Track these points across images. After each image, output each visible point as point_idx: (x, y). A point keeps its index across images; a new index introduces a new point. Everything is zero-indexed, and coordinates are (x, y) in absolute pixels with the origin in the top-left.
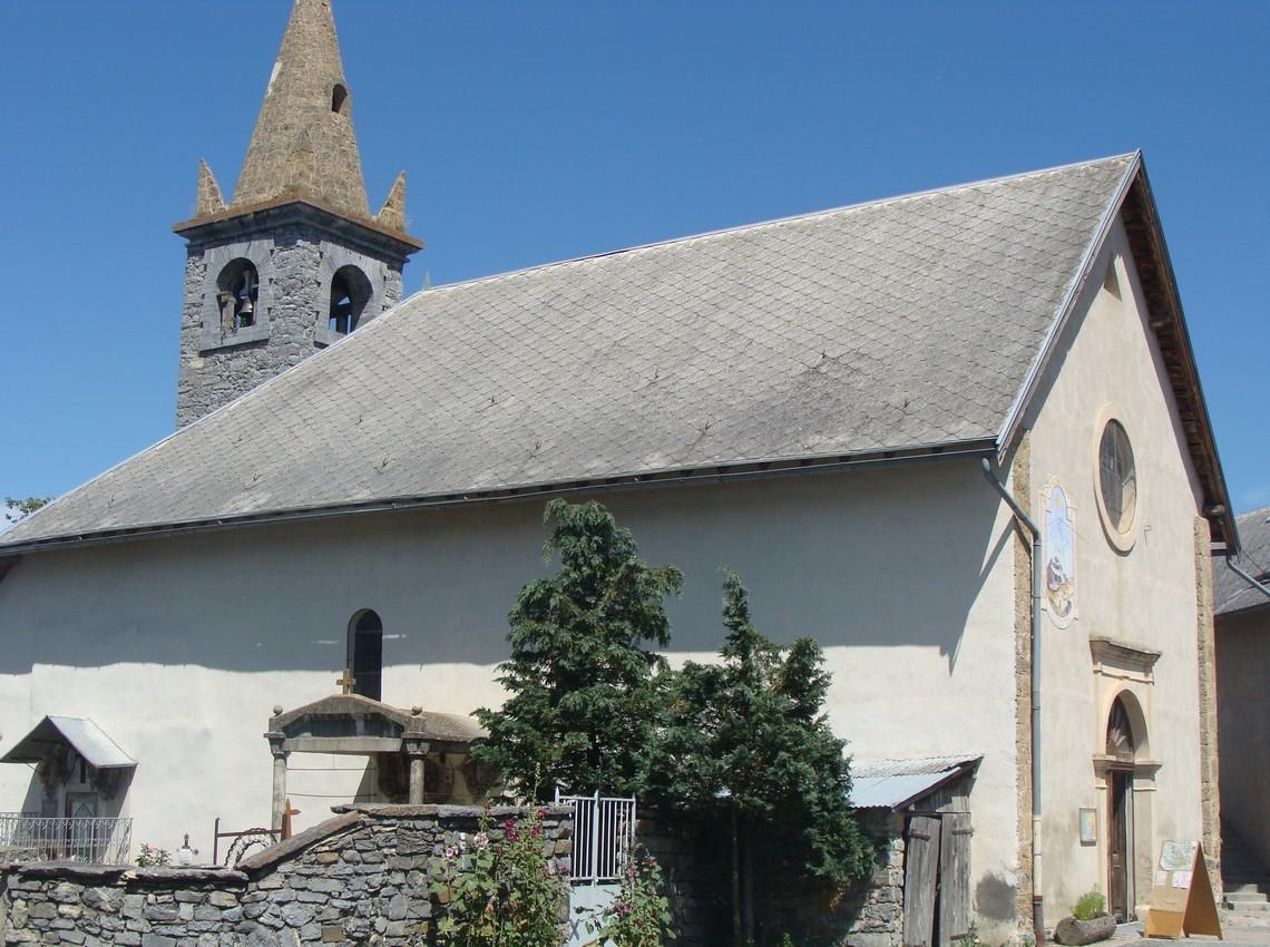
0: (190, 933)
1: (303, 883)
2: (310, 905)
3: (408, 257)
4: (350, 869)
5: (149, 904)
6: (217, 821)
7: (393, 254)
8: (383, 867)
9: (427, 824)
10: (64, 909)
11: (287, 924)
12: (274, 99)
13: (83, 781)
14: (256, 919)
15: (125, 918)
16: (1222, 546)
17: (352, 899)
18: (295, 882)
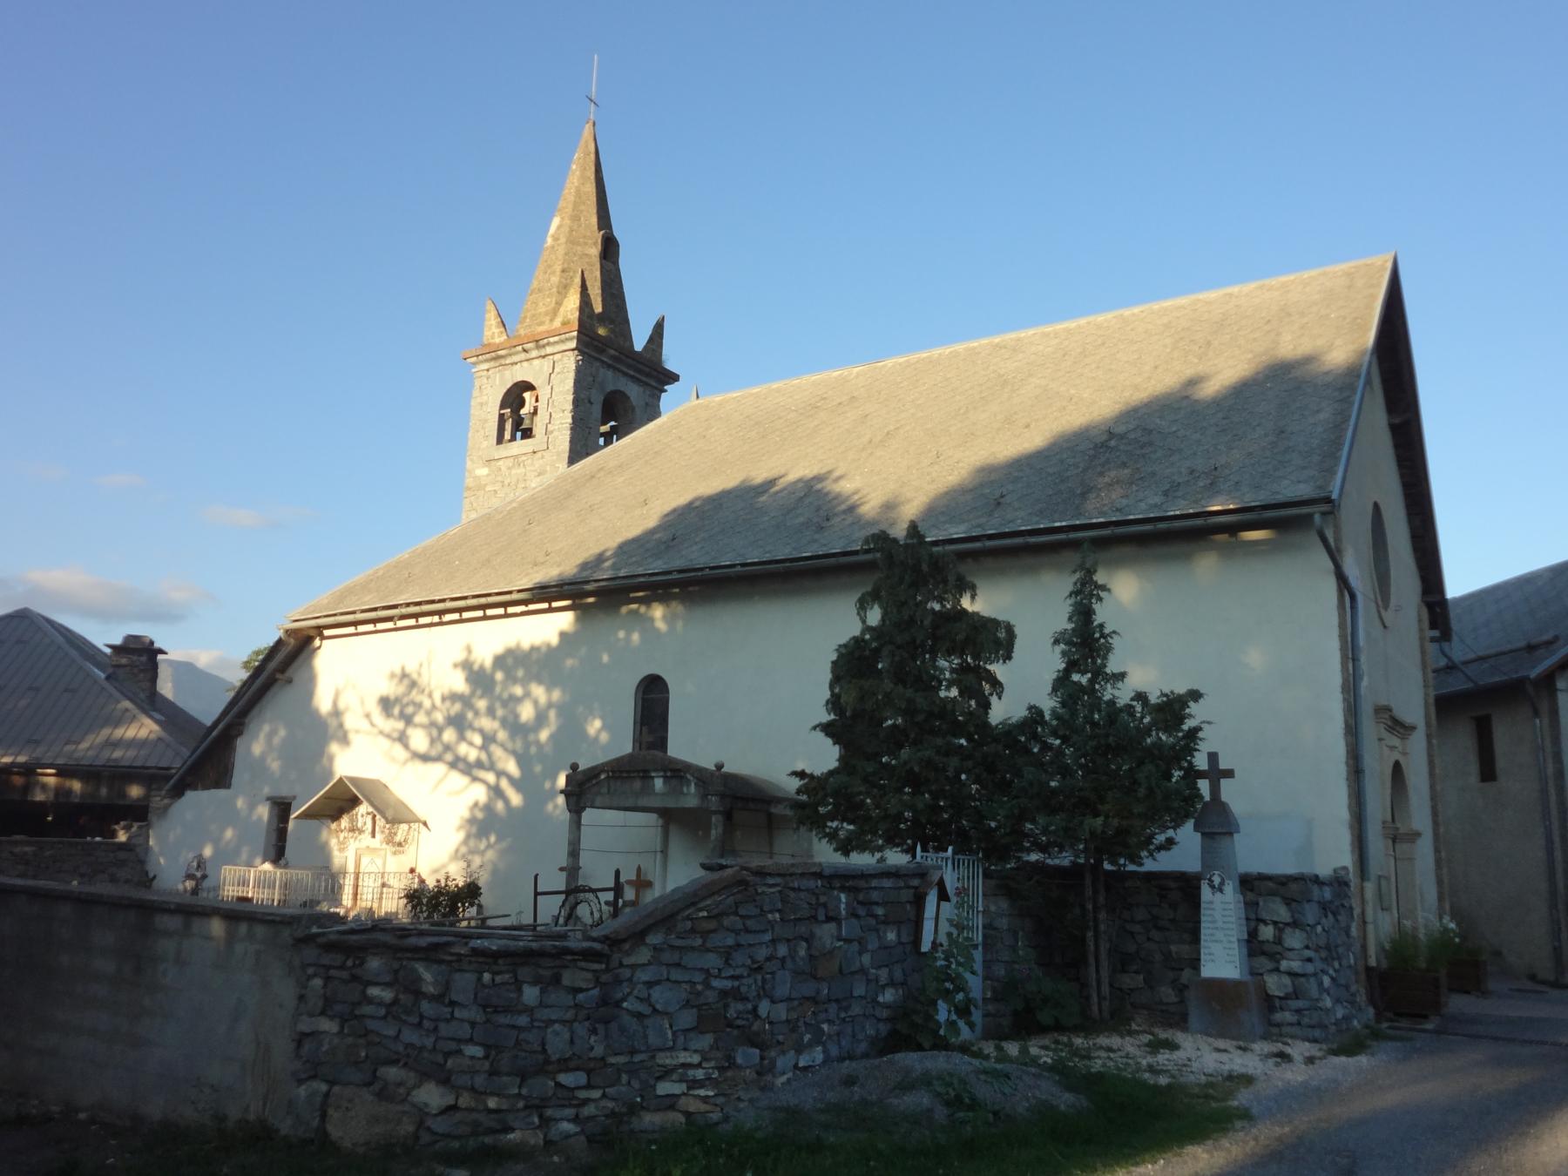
0: (536, 1024)
1: (675, 957)
2: (684, 986)
3: (666, 387)
4: (730, 941)
5: (484, 986)
6: (536, 877)
7: (654, 384)
8: (767, 937)
9: (811, 884)
10: (374, 991)
11: (655, 1010)
12: (553, 247)
13: (373, 835)
14: (618, 1004)
15: (452, 1004)
16: (1436, 633)
17: (733, 977)
18: (667, 957)
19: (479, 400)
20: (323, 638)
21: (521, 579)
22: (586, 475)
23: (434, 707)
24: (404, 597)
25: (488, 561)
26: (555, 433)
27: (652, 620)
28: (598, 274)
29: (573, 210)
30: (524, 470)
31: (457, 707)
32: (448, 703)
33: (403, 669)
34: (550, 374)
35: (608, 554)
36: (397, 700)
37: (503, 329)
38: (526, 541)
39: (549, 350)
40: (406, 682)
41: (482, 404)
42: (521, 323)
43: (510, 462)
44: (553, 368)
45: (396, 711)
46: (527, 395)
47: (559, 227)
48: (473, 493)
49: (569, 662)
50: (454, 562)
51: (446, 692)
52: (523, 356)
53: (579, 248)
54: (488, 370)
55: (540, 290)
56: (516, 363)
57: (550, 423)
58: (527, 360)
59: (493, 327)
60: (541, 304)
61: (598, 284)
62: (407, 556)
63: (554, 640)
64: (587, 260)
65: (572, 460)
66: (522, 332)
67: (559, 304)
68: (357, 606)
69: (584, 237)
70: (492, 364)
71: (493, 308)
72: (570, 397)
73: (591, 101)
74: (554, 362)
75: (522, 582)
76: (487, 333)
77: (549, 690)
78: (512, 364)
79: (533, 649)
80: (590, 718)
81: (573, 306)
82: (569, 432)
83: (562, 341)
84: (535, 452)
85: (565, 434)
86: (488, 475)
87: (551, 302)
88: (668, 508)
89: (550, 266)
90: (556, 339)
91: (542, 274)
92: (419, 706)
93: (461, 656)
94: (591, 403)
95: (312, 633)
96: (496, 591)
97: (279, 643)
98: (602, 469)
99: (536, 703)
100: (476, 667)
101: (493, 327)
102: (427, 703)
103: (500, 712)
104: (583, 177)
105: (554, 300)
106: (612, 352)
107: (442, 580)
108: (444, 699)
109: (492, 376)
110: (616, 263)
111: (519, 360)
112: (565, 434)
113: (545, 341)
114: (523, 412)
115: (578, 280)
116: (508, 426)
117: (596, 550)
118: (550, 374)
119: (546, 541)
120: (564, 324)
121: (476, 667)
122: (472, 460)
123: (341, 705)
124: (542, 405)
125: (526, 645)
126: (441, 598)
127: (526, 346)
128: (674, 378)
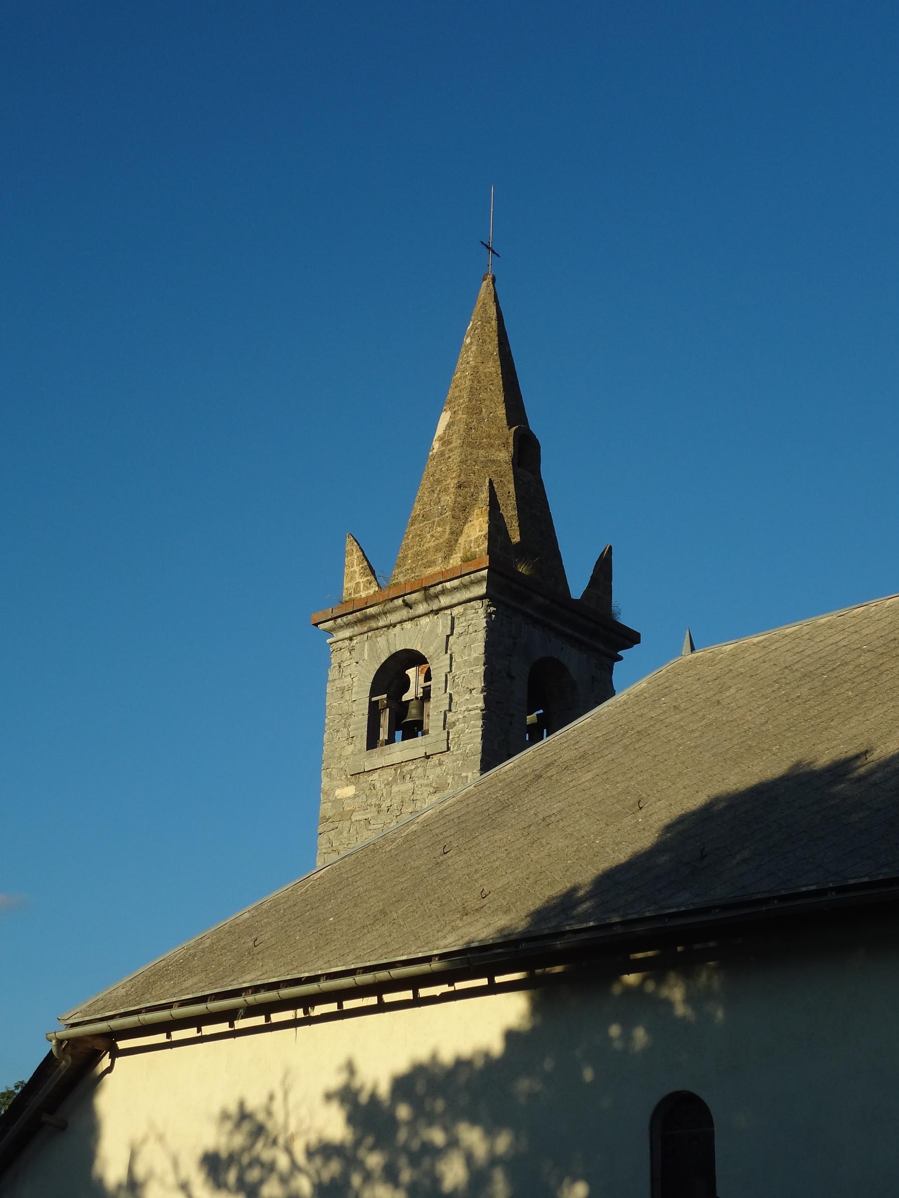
12: (442, 454)
19: (338, 684)
20: (117, 1053)
21: (445, 937)
22: (526, 775)
23: (294, 1165)
24: (249, 977)
25: (384, 912)
26: (460, 726)
27: (669, 1004)
28: (512, 487)
29: (470, 400)
30: (411, 785)
31: (334, 1167)
32: (318, 1161)
33: (242, 1105)
34: (448, 637)
35: (581, 893)
36: (232, 1158)
37: (371, 578)
38: (443, 880)
39: (444, 601)
40: (247, 1126)
41: (343, 690)
42: (399, 566)
43: (388, 775)
44: (452, 628)
45: (232, 1176)
46: (411, 672)
47: (449, 426)
48: (332, 826)
49: (524, 1085)
50: (327, 919)
51: (313, 1138)
52: (404, 613)
53: (482, 452)
54: (351, 639)
55: (425, 517)
56: (394, 626)
57: (450, 710)
58: (411, 619)
59: (357, 576)
60: (429, 536)
61: (513, 501)
62: (247, 915)
63: (496, 1045)
64: (494, 468)
65: (486, 765)
66: (401, 579)
67: (456, 534)
68: (174, 995)
69: (489, 436)
70: (357, 629)
71: (355, 547)
72: (481, 669)
73: (488, 247)
74: (453, 619)
75: (447, 942)
76: (348, 585)
77: (490, 1133)
78: (387, 627)
79: (461, 1064)
80: (567, 1181)
81: (480, 533)
82: (480, 723)
83: (465, 586)
84: (428, 757)
85: (474, 726)
86: (355, 796)
87: (443, 532)
88: (677, 811)
89: (439, 481)
90: (456, 583)
91: (427, 494)
92: (270, 1168)
93: (335, 1081)
94: (512, 678)
95: (99, 1044)
96: (404, 958)
97: (49, 1061)
98: (552, 763)
99: (469, 1159)
100: (364, 1098)
101: (357, 576)
102: (283, 1162)
103: (406, 1176)
104: (482, 353)
105: (448, 528)
106: (540, 600)
107: (310, 947)
108: (310, 1154)
109: (358, 646)
110: (536, 472)
111: (399, 619)
112: (474, 726)
113: (439, 587)
114: (406, 697)
115: (484, 495)
116: (385, 721)
117: (562, 886)
118: (448, 637)
119: (476, 877)
120: (466, 560)
121: (364, 1098)
122: (330, 775)
123: (140, 1171)
124: (436, 683)
125: (447, 1056)
126: (312, 974)
127: (410, 598)
128: (631, 638)
